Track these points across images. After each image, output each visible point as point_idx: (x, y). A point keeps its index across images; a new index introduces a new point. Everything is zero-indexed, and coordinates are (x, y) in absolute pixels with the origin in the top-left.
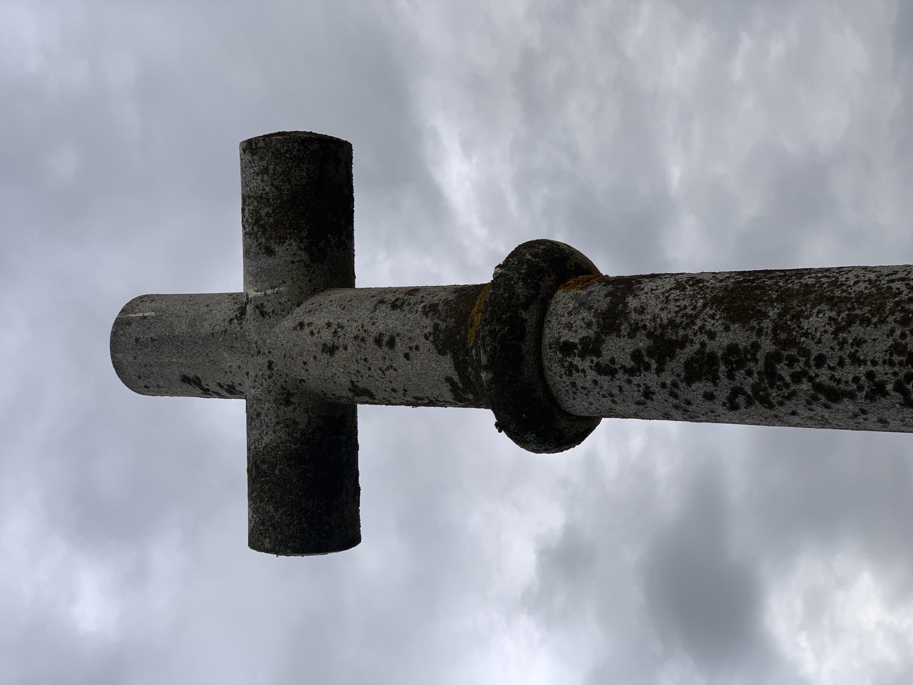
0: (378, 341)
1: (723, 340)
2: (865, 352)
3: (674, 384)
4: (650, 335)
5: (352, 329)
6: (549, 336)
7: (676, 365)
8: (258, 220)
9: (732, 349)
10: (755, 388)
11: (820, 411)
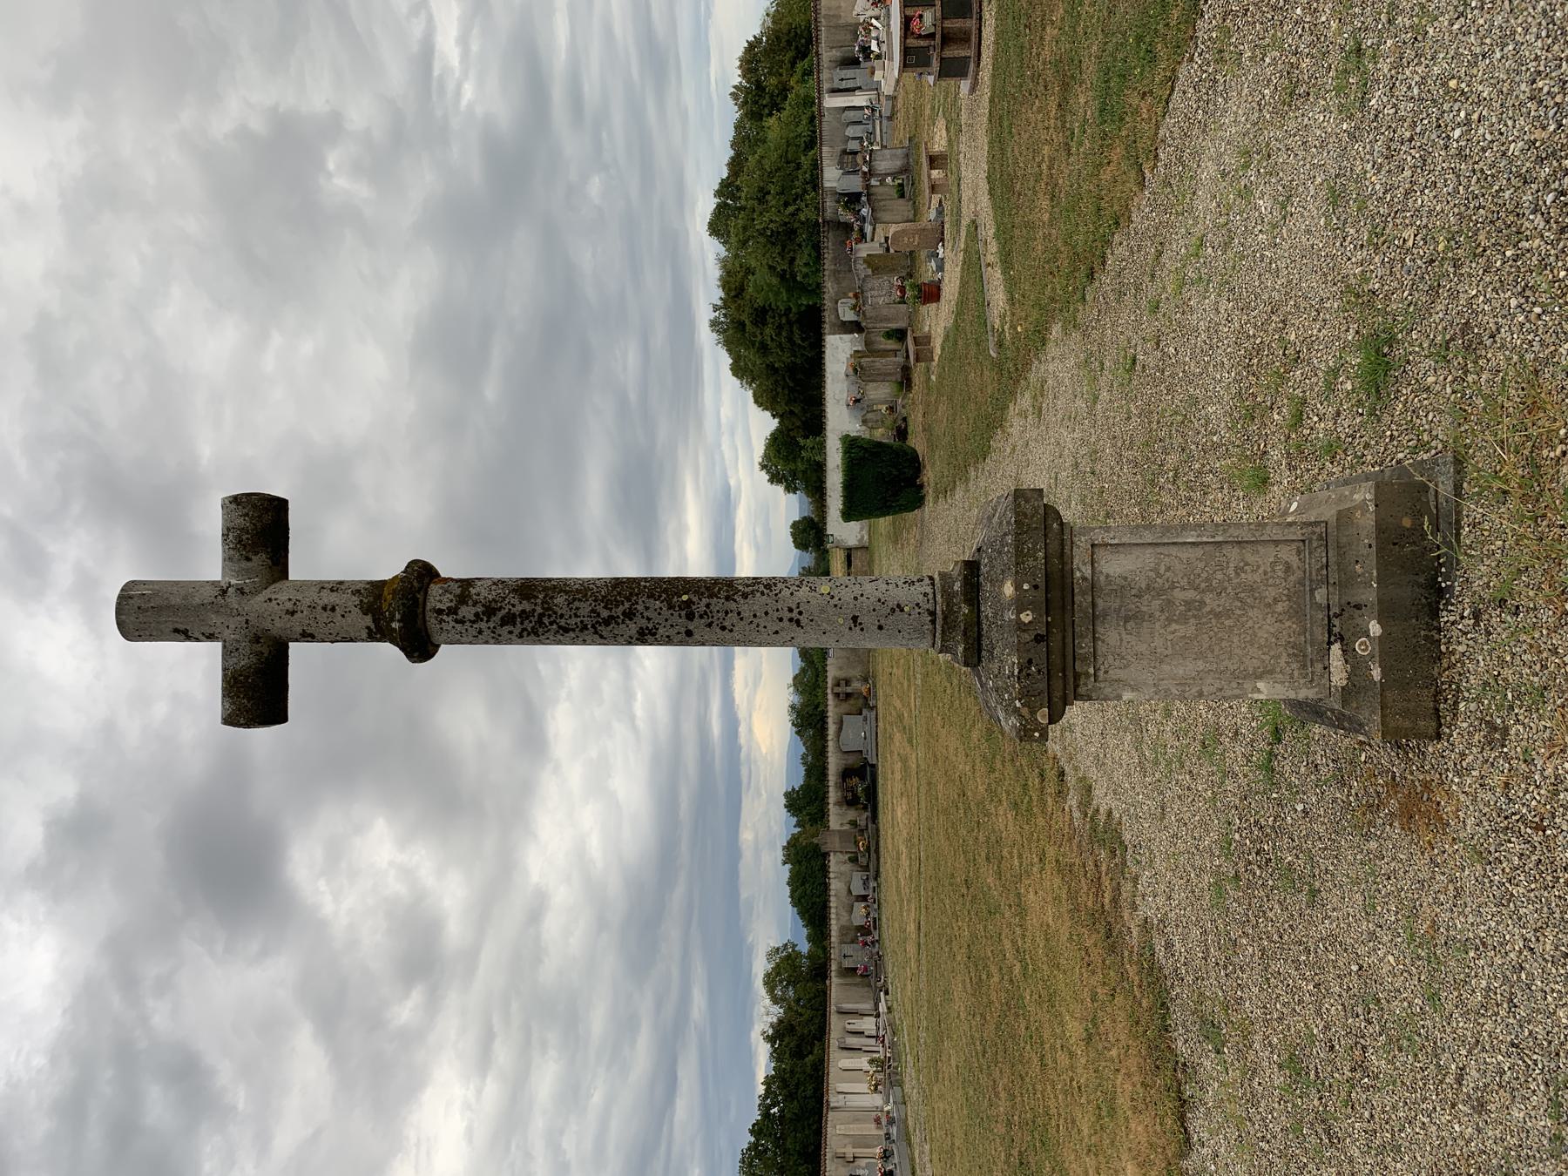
0: (324, 608)
1: (519, 608)
2: (580, 612)
3: (495, 627)
4: (483, 605)
5: (307, 601)
6: (429, 606)
7: (497, 618)
8: (240, 542)
9: (523, 611)
10: (533, 628)
11: (559, 637)
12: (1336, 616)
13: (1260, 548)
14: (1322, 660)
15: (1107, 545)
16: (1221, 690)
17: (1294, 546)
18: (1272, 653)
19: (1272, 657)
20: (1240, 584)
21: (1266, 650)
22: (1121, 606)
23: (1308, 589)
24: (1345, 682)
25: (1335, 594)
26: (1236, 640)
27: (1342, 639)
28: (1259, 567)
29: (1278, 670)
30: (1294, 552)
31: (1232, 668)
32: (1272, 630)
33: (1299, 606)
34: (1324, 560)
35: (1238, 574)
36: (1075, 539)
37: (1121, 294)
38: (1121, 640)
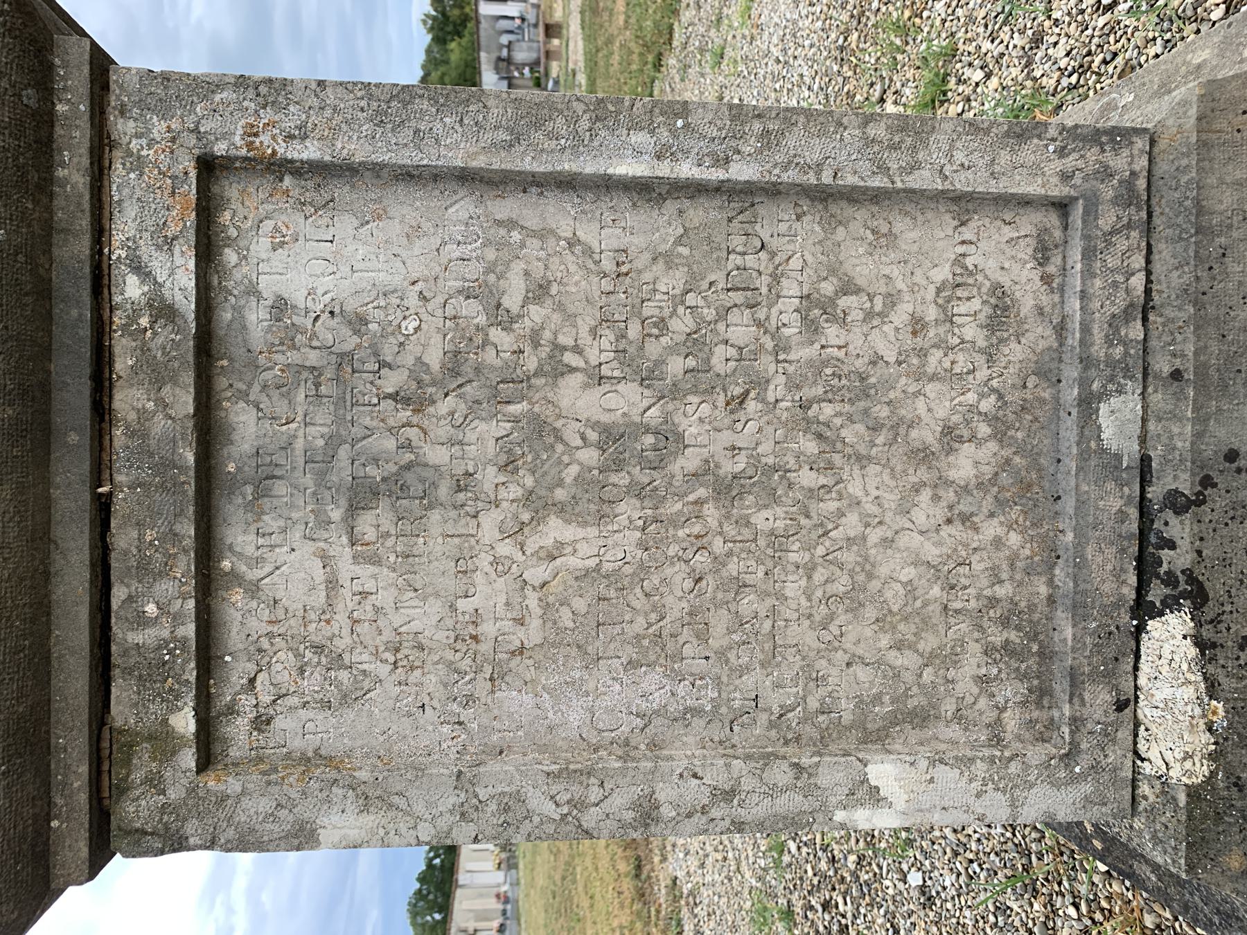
12: (1178, 503)
13: (900, 224)
14: (1109, 676)
15: (278, 167)
16: (729, 795)
17: (1028, 223)
18: (929, 643)
19: (929, 660)
20: (818, 367)
21: (906, 630)
22: (334, 442)
23: (1071, 394)
24: (1202, 770)
25: (1175, 417)
26: (793, 587)
27: (1197, 596)
28: (892, 300)
29: (949, 707)
30: (1025, 250)
31: (774, 700)
32: (931, 552)
33: (1033, 456)
34: (1138, 282)
35: (812, 328)
36: (123, 128)
37: (686, 67)
38: (332, 584)
